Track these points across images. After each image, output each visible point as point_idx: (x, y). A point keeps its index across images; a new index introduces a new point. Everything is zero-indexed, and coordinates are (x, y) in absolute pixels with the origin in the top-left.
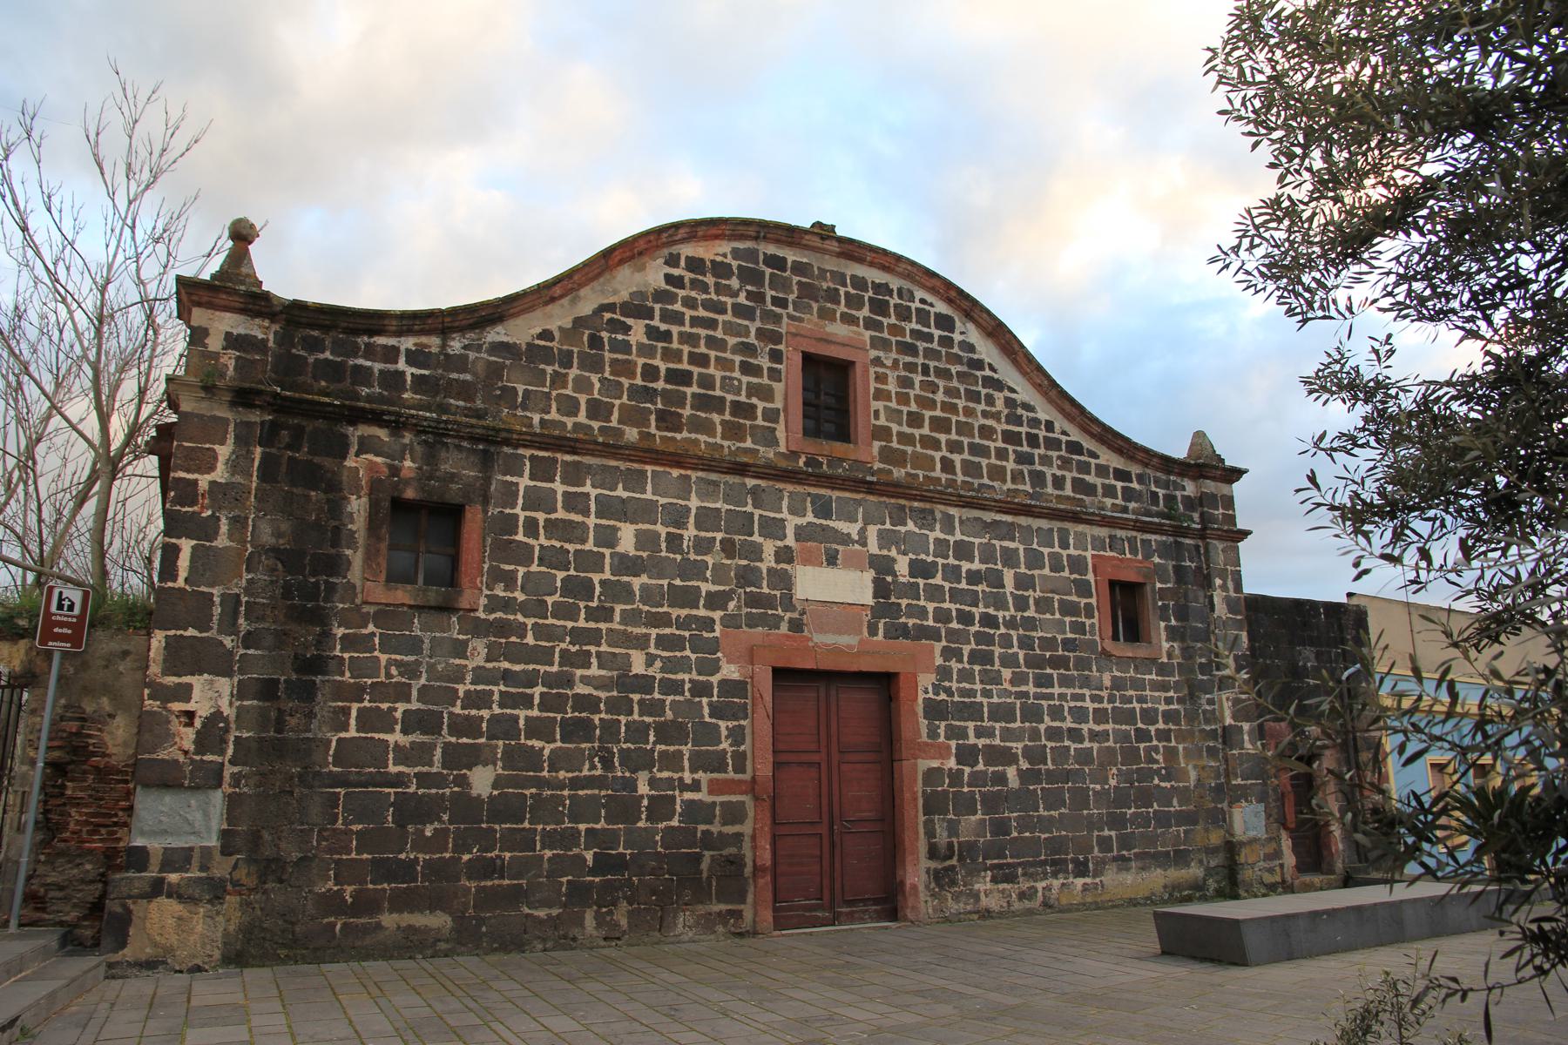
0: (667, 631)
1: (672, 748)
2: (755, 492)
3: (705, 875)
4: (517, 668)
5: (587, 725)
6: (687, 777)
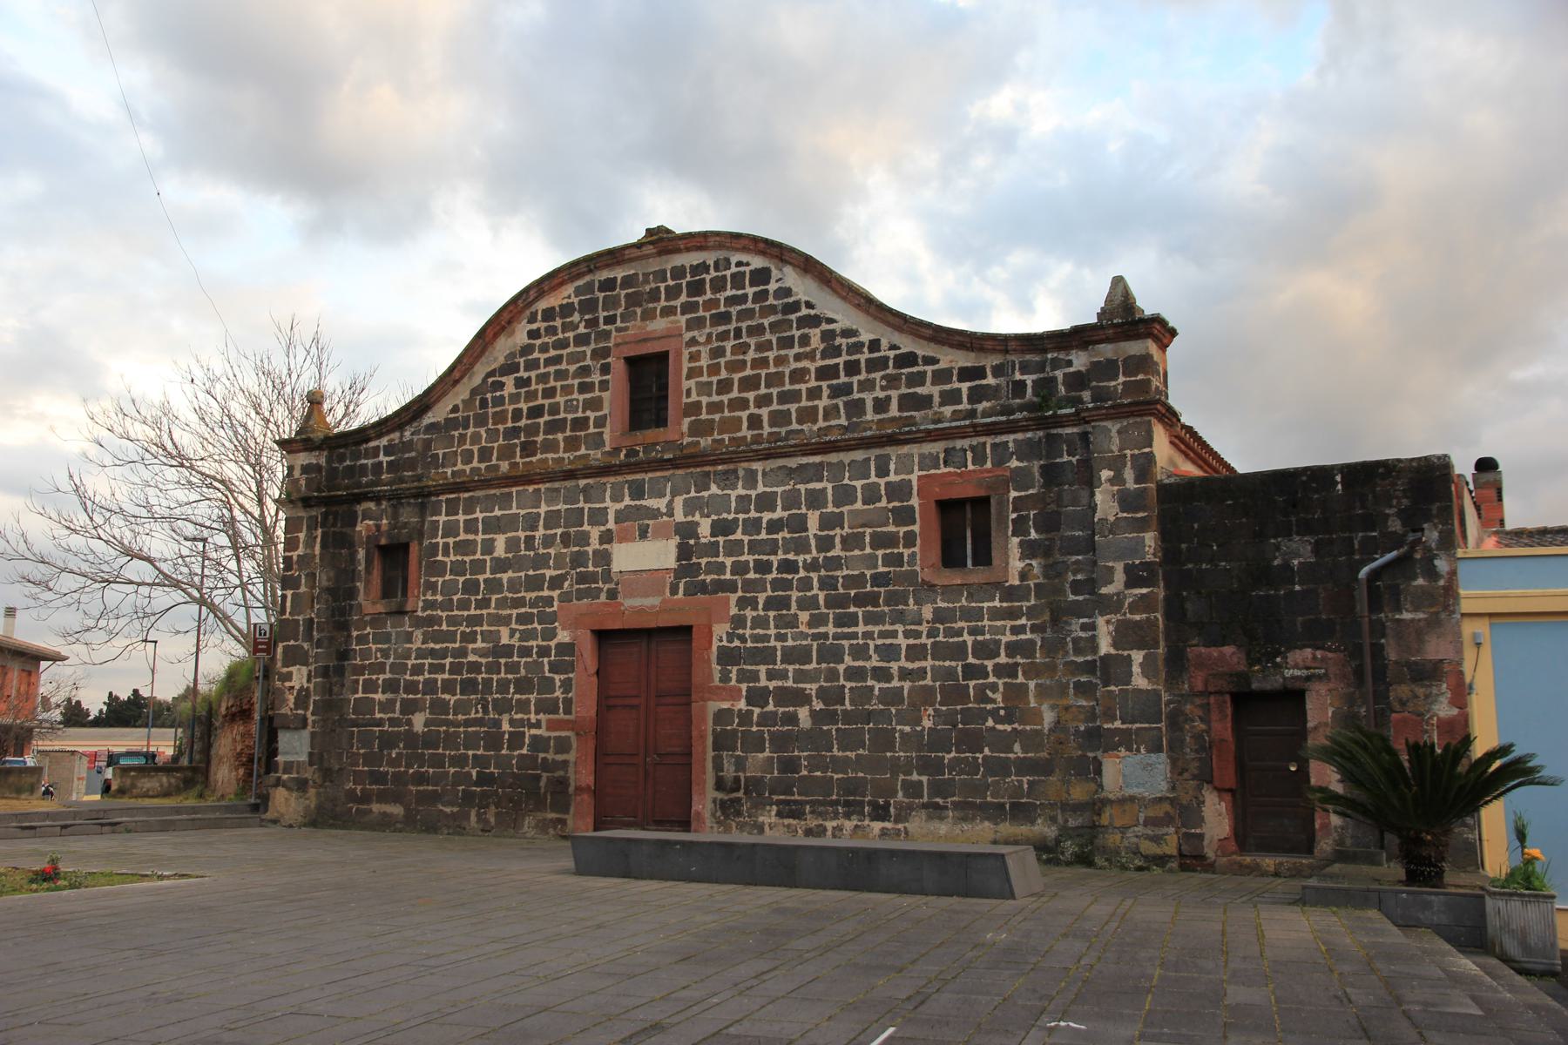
2: (585, 490)
5: (474, 682)
6: (533, 718)
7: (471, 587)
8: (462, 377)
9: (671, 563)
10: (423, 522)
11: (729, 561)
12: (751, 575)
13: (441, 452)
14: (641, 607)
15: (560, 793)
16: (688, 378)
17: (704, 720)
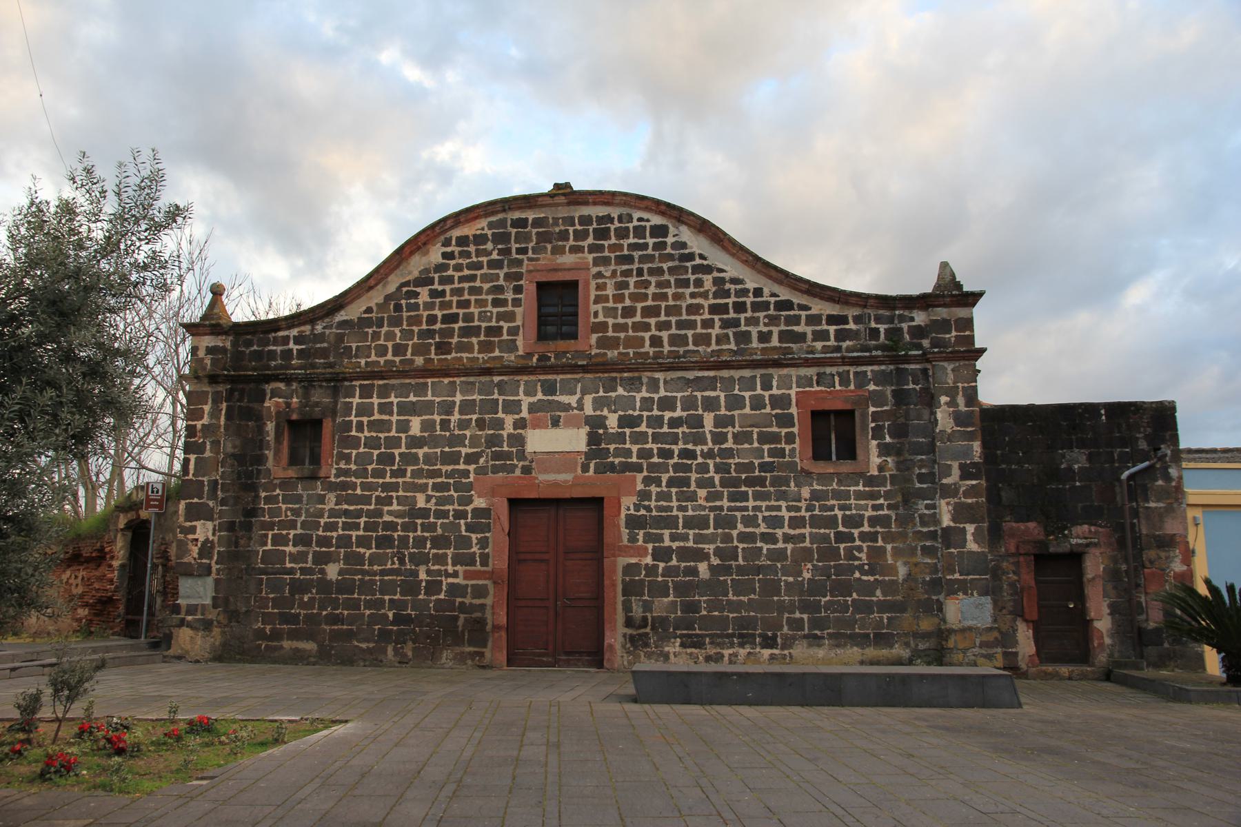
0: (439, 480)
2: (500, 385)
4: (352, 508)
5: (391, 538)
6: (450, 569)
7: (387, 459)
8: (376, 285)
9: (582, 446)
10: (336, 403)
11: (635, 448)
12: (655, 460)
13: (354, 345)
14: (550, 481)
15: (478, 631)
16: (596, 302)
17: (614, 571)
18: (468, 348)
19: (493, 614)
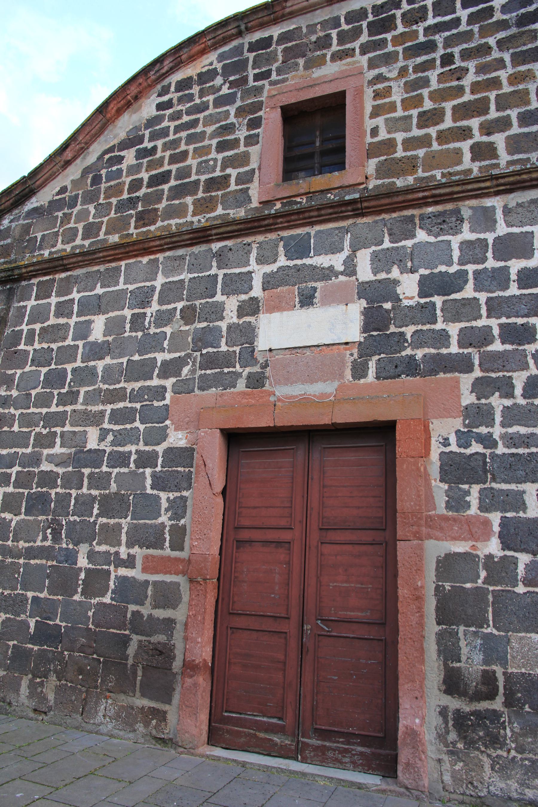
0: (121, 405)
1: (112, 521)
2: (219, 255)
3: (130, 662)
5: (44, 498)
6: (123, 552)
7: (56, 379)
8: (75, 158)
9: (353, 332)
10: (8, 310)
11: (454, 329)
12: (497, 346)
13: (39, 235)
14: (296, 398)
15: (158, 671)
16: (374, 114)
17: (419, 570)
18: (181, 211)
19: (186, 639)
